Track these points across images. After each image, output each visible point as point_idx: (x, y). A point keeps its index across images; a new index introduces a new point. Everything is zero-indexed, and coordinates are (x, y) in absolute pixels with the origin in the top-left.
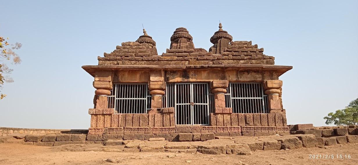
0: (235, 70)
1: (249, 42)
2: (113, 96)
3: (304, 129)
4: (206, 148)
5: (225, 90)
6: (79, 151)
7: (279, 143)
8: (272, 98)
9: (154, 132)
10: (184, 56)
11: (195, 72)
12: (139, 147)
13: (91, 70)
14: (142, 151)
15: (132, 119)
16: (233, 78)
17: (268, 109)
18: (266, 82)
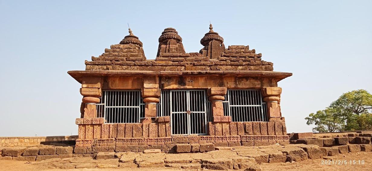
0: (234, 76)
1: (246, 47)
2: (102, 104)
3: (306, 138)
4: (211, 163)
5: (223, 98)
6: (69, 168)
7: (284, 155)
8: (272, 106)
9: (149, 143)
10: (180, 61)
11: (192, 78)
12: (135, 162)
13: (77, 76)
14: (141, 166)
15: (124, 129)
16: (231, 84)
17: (267, 118)
18: (266, 89)
